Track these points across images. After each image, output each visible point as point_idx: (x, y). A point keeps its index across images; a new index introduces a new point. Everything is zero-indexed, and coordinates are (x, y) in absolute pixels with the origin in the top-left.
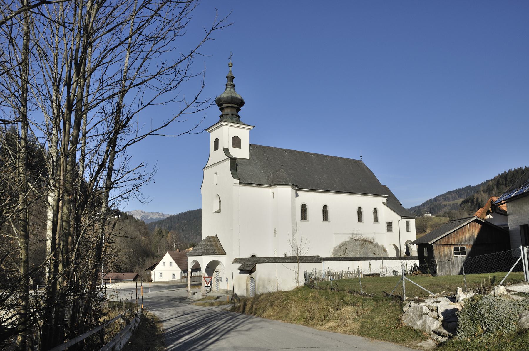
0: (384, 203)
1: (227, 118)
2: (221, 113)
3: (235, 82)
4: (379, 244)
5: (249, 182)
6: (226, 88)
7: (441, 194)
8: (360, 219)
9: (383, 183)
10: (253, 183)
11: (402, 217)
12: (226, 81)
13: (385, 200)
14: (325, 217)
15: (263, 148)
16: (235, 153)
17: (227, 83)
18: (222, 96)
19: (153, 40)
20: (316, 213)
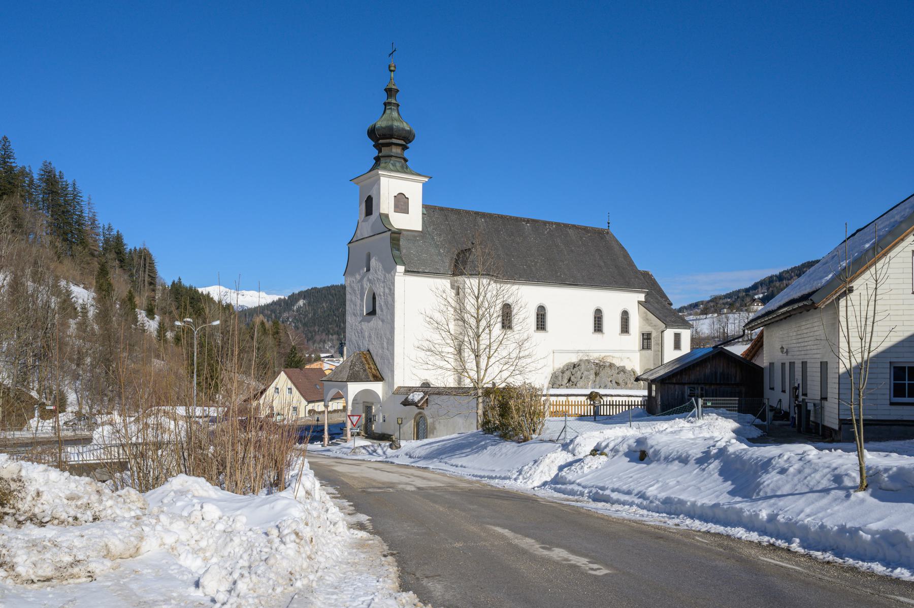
0: (639, 302)
1: (385, 163)
2: (375, 153)
3: (399, 99)
4: (626, 368)
5: (420, 270)
6: (385, 108)
7: (793, 267)
8: (598, 326)
9: (641, 267)
10: (426, 271)
11: (667, 326)
12: (384, 97)
13: (642, 297)
14: (541, 324)
15: (444, 211)
16: (399, 221)
17: (387, 101)
18: (378, 125)
19: (485, 384)
20: (525, 318)
